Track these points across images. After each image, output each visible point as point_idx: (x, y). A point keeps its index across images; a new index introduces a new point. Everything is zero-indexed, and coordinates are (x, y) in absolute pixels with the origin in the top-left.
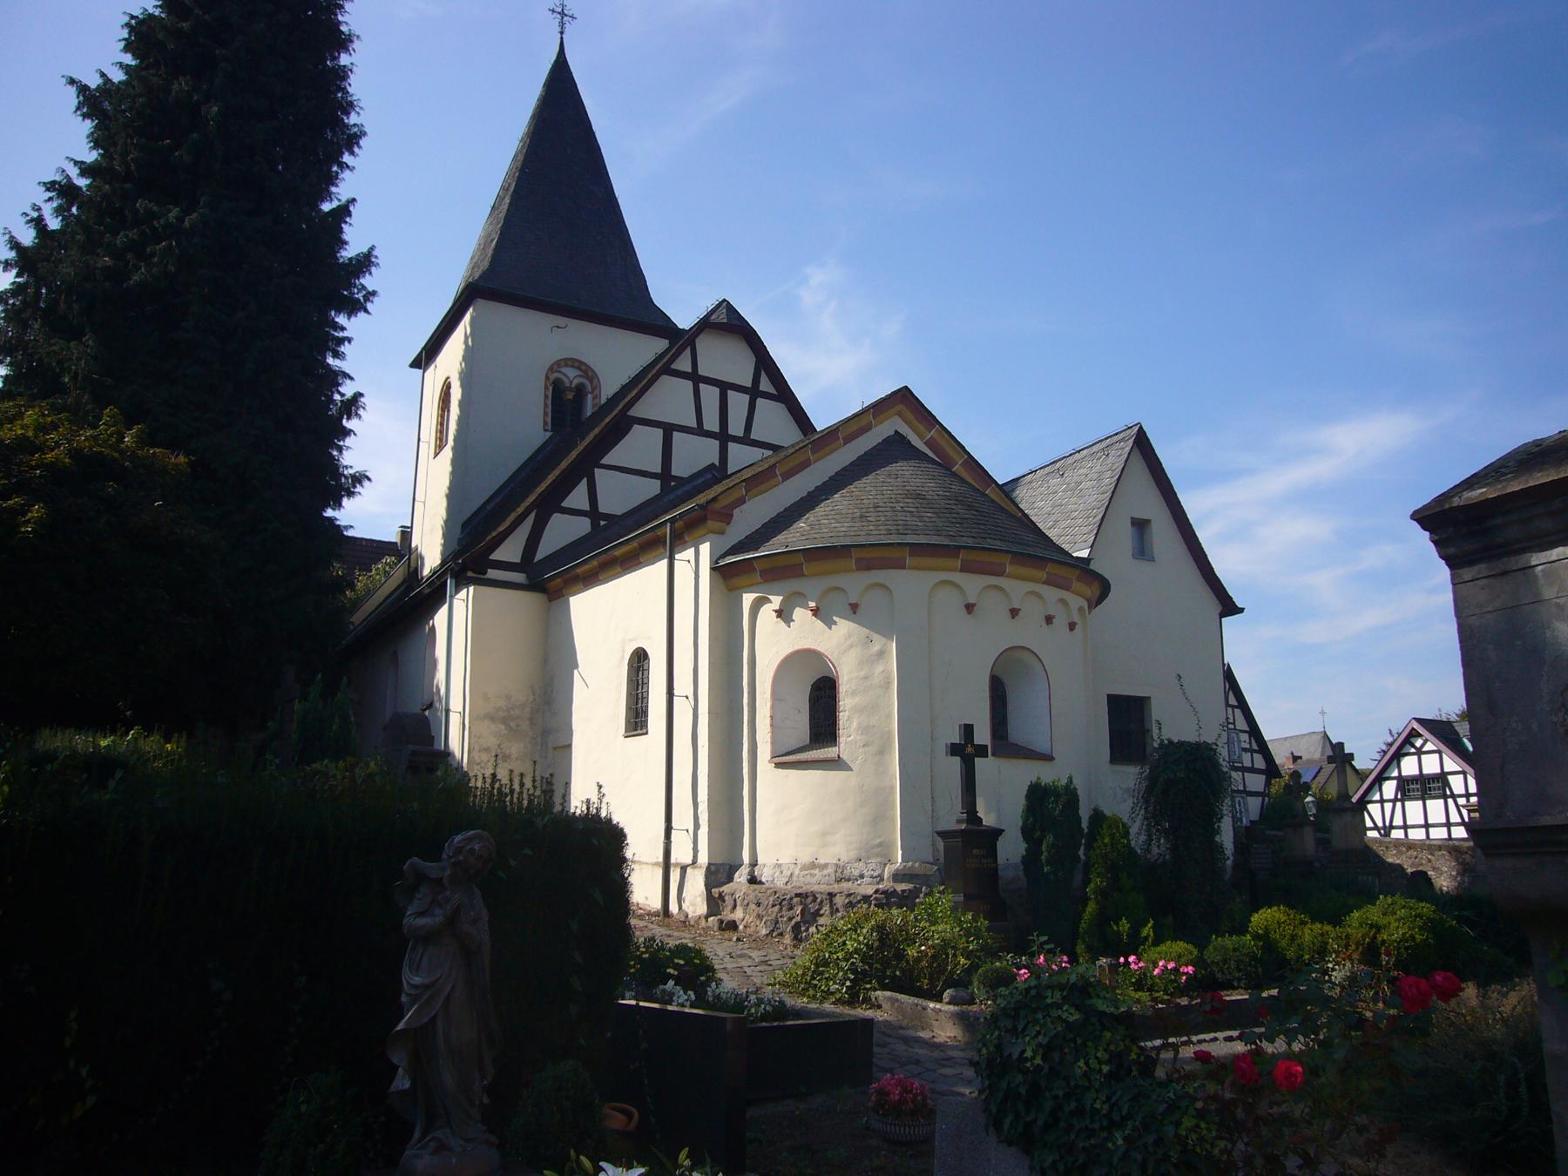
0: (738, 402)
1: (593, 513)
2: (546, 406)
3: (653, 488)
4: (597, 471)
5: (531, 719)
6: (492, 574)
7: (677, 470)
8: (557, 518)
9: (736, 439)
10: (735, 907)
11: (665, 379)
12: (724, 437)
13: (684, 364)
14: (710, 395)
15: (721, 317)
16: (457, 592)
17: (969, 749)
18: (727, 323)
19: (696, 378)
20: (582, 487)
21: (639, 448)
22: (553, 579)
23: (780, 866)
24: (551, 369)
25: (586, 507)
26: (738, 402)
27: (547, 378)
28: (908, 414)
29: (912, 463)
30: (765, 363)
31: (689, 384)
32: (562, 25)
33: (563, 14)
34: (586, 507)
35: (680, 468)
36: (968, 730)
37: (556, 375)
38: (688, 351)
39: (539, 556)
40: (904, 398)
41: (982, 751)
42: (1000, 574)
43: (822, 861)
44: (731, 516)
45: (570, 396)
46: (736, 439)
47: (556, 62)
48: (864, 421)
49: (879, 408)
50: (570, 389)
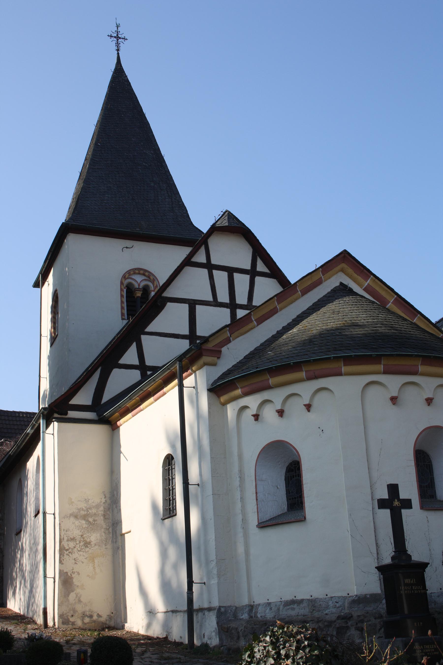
0: (242, 282)
1: (142, 367)
2: (122, 302)
3: (185, 345)
4: (143, 337)
5: (104, 516)
6: (72, 414)
7: (199, 333)
8: (116, 372)
9: (242, 307)
10: (238, 638)
11: (188, 270)
12: (233, 306)
13: (201, 258)
14: (221, 278)
15: (225, 223)
16: (47, 426)
17: (396, 503)
18: (232, 227)
19: (209, 266)
20: (133, 348)
21: (172, 318)
22: (107, 414)
23: (269, 604)
24: (124, 277)
25: (136, 362)
26: (242, 282)
27: (122, 283)
28: (350, 271)
29: (347, 299)
30: (259, 252)
31: (205, 271)
32: (118, 45)
33: (118, 38)
34: (136, 362)
35: (203, 330)
36: (393, 489)
37: (129, 280)
38: (203, 249)
39: (106, 398)
40: (345, 258)
41: (407, 504)
42: (415, 373)
43: (299, 597)
44: (221, 351)
45: (139, 294)
46: (242, 307)
47: (116, 69)
48: (315, 278)
49: (327, 267)
50: (139, 289)
